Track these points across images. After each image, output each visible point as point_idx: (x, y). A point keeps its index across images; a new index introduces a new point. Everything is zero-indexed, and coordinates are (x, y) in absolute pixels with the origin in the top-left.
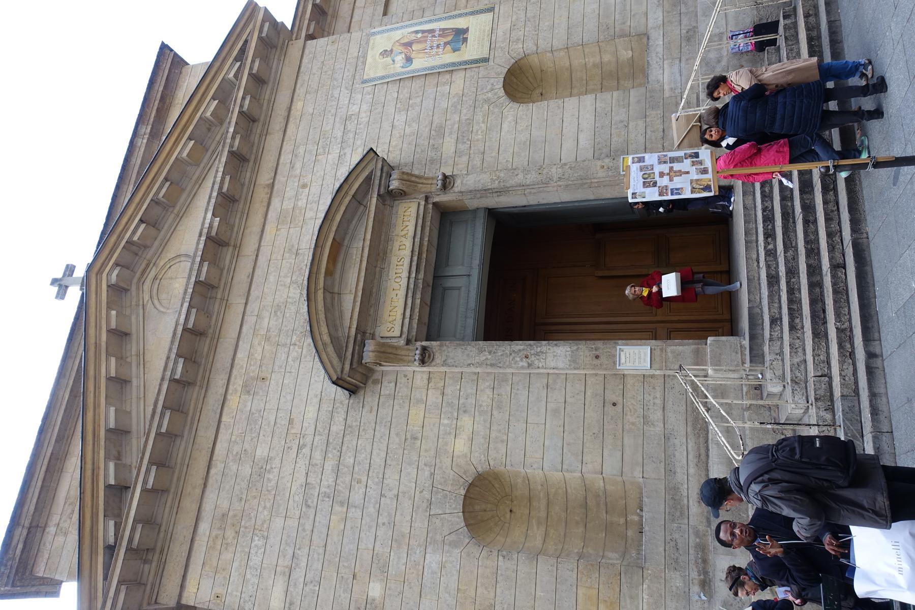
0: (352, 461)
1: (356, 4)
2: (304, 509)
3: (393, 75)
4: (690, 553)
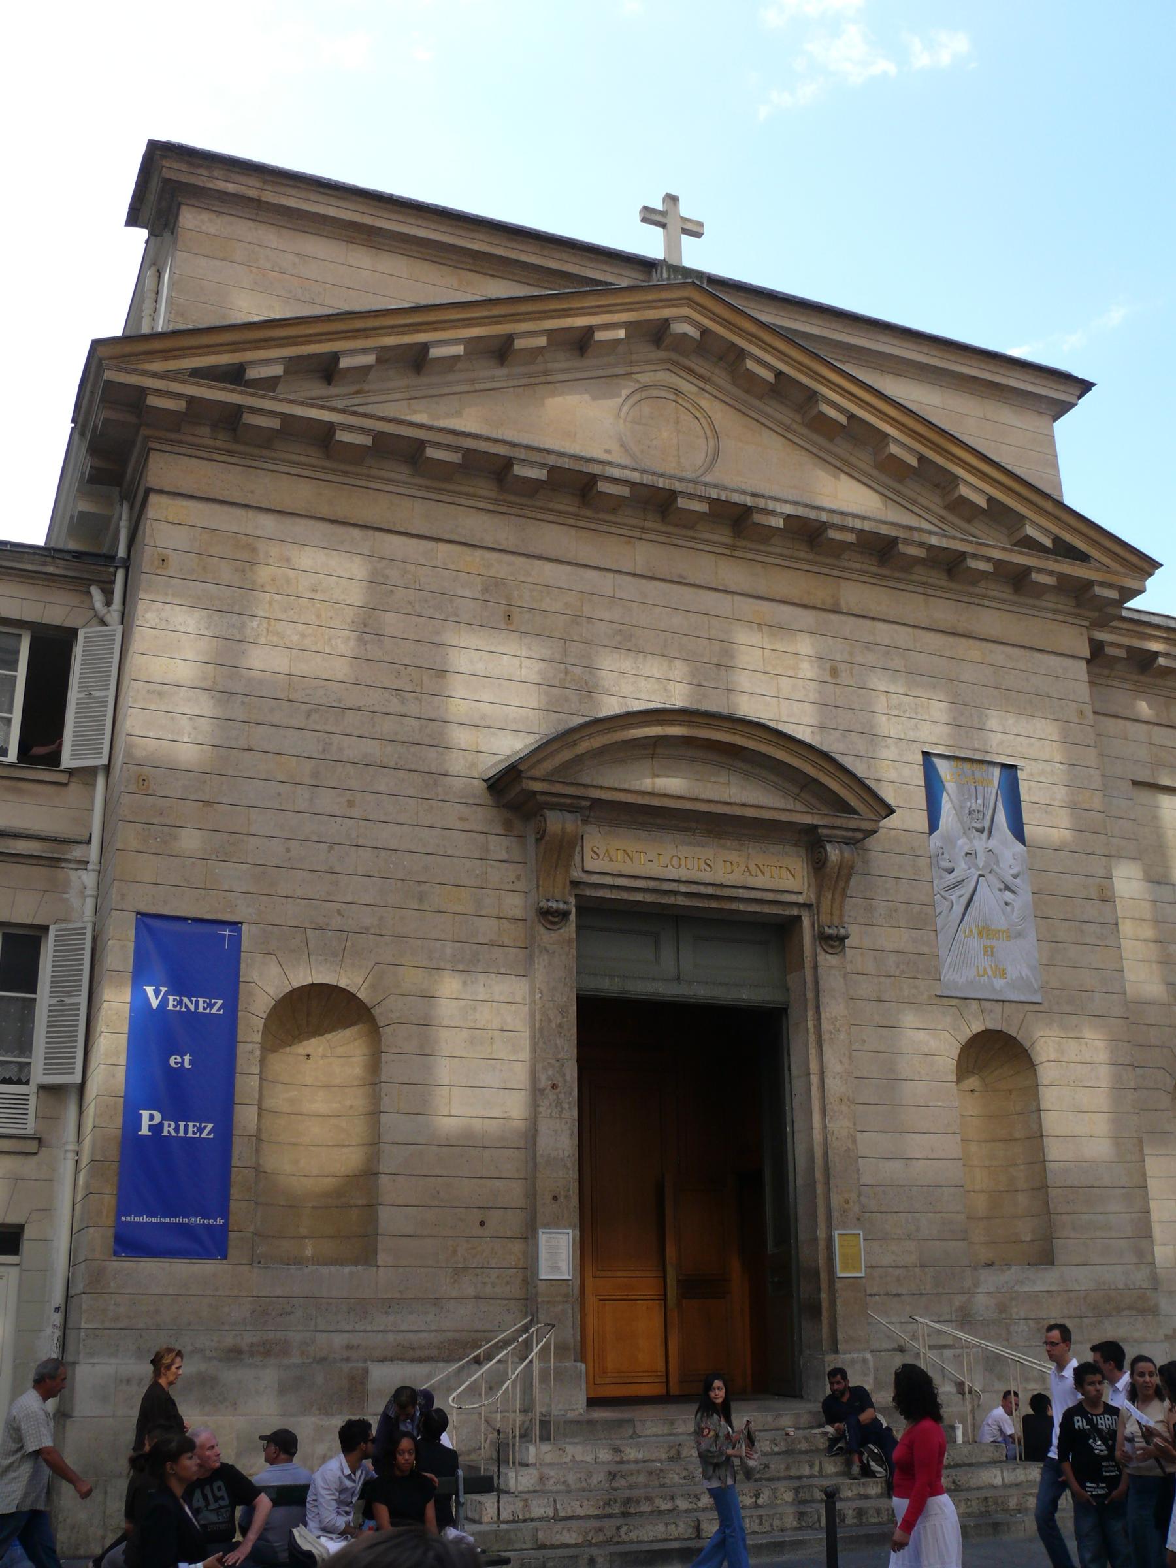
0: (382, 788)
4: (279, 1333)
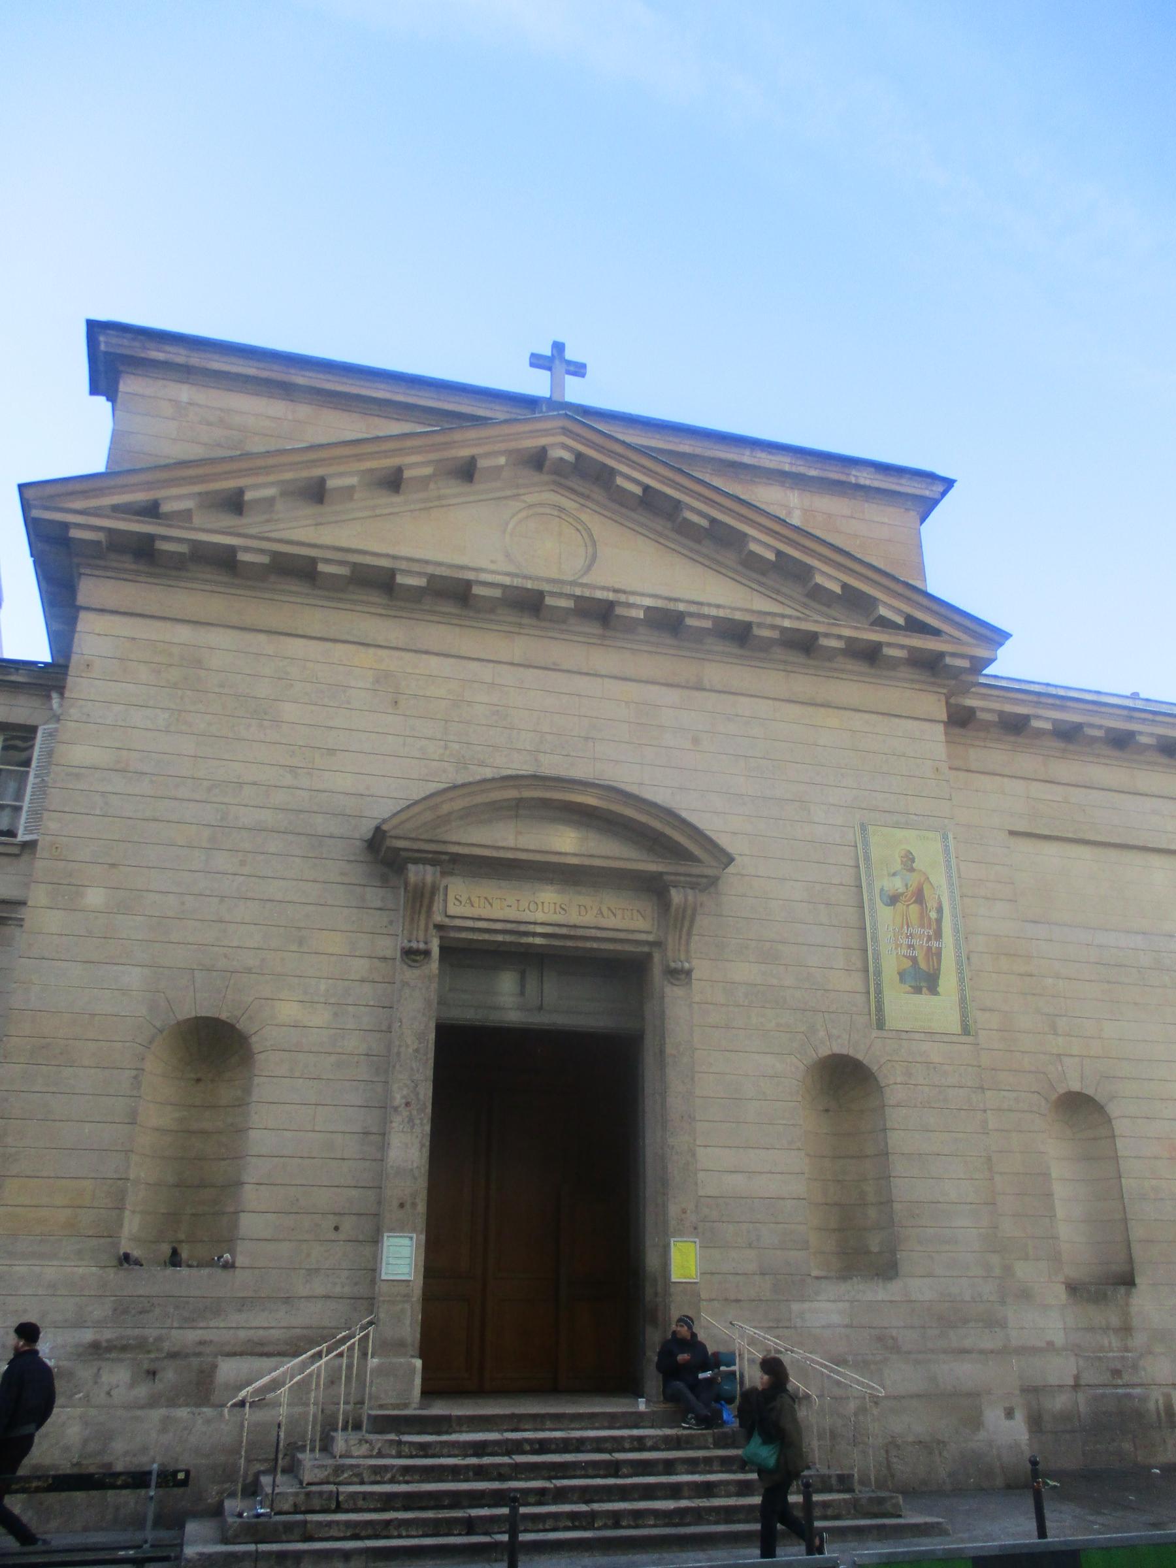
0: (272, 850)
1: (1034, 783)
2: (206, 783)
3: (869, 876)
